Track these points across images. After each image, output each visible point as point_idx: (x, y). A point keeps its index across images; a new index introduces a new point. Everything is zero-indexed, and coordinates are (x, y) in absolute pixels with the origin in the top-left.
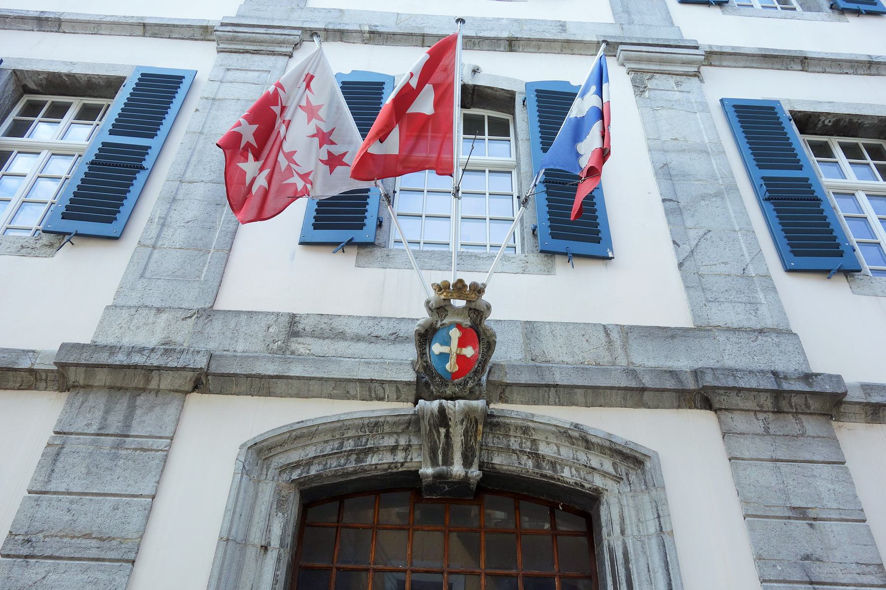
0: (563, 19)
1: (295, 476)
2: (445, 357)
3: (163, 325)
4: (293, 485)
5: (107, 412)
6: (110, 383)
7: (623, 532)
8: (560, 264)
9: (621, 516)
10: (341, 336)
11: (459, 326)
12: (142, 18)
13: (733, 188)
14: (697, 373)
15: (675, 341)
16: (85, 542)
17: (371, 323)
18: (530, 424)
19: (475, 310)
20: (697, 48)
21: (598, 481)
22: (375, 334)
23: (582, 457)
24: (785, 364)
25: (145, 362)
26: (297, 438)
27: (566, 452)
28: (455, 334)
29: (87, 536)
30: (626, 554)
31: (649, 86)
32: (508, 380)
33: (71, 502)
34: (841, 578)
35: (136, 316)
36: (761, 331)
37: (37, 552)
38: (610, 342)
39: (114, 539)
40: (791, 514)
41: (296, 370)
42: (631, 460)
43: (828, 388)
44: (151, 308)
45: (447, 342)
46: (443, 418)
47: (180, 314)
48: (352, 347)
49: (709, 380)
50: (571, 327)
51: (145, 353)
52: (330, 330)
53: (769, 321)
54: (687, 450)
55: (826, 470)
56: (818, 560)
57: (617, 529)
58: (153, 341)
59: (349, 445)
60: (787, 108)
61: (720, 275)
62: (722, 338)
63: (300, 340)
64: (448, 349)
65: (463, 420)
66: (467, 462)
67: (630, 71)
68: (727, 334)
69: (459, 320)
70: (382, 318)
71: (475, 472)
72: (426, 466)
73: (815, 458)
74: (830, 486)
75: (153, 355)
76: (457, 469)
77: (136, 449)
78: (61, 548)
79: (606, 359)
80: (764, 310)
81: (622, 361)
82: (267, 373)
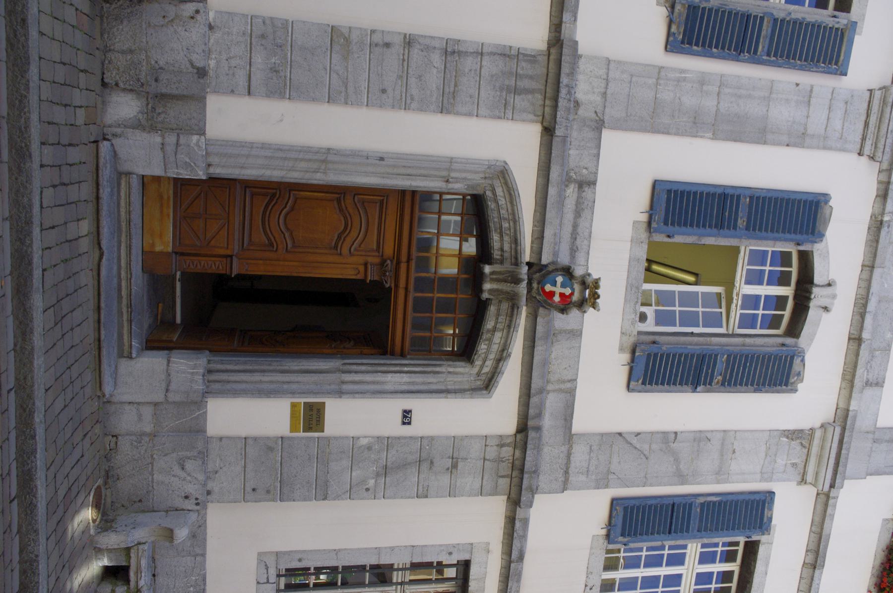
0: (885, 385)
1: (489, 193)
2: (554, 284)
5: (531, 78)
6: (546, 81)
7: (449, 372)
8: (626, 357)
9: (462, 373)
10: (578, 213)
11: (572, 294)
13: (683, 480)
14: (538, 429)
16: (453, 84)
17: (586, 234)
21: (478, 363)
23: (492, 356)
24: (543, 480)
26: (510, 194)
27: (495, 348)
28: (568, 291)
29: (456, 85)
30: (438, 373)
34: (422, 476)
36: (566, 472)
37: (449, 58)
38: (564, 382)
41: (552, 191)
42: (488, 385)
43: (523, 499)
45: (563, 285)
46: (517, 281)
47: (599, 109)
52: (582, 208)
53: (572, 478)
54: (492, 415)
55: (477, 485)
57: (451, 370)
58: (580, 95)
59: (505, 225)
60: (763, 539)
62: (564, 449)
63: (576, 190)
64: (558, 287)
66: (491, 291)
68: (566, 452)
70: (590, 242)
71: (485, 296)
75: (566, 101)
76: (487, 286)
77: (506, 100)
81: (550, 387)
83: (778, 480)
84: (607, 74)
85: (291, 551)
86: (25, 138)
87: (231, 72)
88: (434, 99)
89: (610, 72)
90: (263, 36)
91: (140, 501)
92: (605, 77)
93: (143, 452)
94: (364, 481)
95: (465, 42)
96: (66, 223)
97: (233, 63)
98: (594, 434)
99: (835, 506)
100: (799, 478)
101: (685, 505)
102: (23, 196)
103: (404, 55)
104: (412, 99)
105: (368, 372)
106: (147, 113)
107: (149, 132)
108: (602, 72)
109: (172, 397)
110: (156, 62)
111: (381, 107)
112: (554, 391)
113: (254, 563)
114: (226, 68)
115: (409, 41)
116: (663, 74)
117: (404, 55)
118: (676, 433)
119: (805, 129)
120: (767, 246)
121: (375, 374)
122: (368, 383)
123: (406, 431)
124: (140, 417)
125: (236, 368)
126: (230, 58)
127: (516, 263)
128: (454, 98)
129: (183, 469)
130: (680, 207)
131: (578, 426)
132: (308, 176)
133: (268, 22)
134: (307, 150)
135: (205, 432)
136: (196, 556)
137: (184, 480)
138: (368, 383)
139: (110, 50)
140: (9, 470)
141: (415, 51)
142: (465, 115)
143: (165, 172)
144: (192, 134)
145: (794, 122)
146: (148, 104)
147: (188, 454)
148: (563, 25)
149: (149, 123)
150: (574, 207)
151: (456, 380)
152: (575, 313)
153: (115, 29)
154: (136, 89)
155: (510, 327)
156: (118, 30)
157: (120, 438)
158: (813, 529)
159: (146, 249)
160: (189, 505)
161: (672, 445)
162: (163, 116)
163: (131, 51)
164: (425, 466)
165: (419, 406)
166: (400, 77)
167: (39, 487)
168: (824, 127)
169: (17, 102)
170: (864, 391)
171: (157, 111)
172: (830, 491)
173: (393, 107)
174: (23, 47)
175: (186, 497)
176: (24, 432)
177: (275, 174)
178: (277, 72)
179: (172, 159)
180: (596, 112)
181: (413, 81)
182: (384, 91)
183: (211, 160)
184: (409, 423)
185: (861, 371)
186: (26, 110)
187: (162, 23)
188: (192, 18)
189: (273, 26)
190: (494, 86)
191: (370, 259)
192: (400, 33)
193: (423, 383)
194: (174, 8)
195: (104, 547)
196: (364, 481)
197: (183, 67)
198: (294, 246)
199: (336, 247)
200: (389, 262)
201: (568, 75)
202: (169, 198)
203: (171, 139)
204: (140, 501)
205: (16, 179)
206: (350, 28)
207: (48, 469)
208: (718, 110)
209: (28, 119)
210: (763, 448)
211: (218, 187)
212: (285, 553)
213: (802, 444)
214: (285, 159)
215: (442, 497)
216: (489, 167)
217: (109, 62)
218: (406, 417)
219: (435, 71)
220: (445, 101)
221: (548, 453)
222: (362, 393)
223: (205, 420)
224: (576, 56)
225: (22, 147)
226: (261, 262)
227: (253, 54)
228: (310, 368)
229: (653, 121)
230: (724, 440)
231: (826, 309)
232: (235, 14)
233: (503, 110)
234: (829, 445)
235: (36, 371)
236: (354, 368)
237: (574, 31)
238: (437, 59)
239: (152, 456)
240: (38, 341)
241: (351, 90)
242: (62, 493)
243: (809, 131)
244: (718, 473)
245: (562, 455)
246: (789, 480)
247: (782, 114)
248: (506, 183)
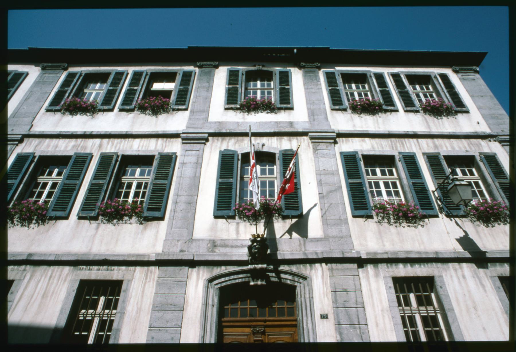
0: (292, 121)
17: (235, 241)
29: (171, 305)
88: (177, 314)
112: (305, 248)
118: (319, 194)
120: (147, 199)
123: (331, 316)
130: (227, 204)
161: (324, 195)
164: (347, 305)
166: (167, 330)
181: (169, 325)
184: (327, 315)
208: (186, 195)
218: (324, 316)
220: (178, 309)
233: (184, 284)
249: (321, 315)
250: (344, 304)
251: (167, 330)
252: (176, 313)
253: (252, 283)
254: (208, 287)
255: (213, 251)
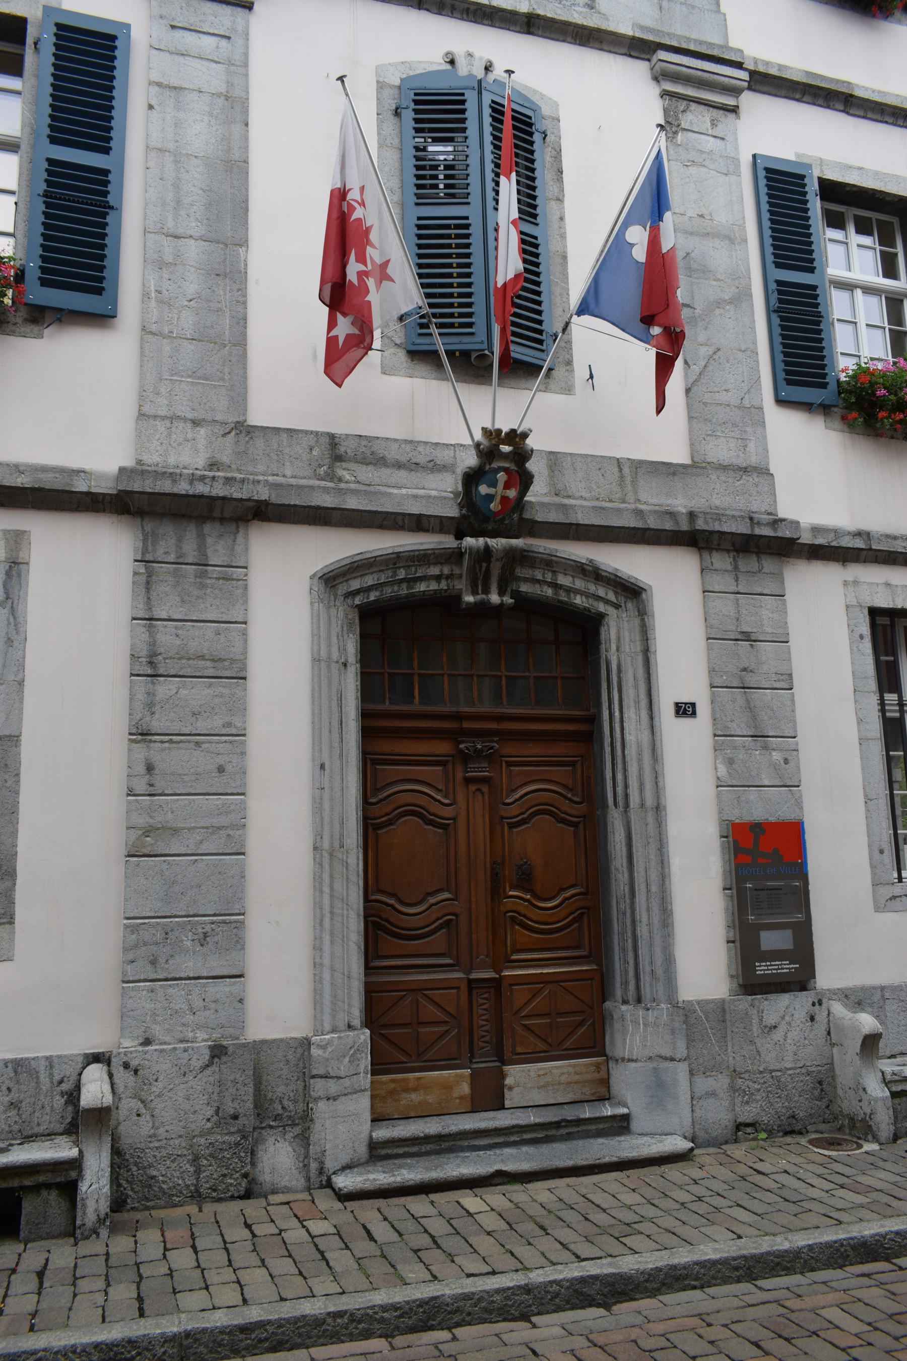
1: (357, 601)
2: (490, 498)
3: (204, 442)
4: (356, 610)
6: (181, 517)
9: (617, 631)
10: (380, 461)
11: (506, 470)
12: (617, 570)
13: (743, 296)
14: (692, 516)
15: (676, 478)
17: (408, 448)
18: (554, 558)
19: (520, 454)
20: (739, 65)
21: (602, 607)
22: (414, 460)
23: (592, 588)
24: (758, 505)
25: (210, 492)
27: (579, 584)
28: (502, 476)
29: (202, 657)
31: (683, 126)
32: (540, 517)
33: (176, 628)
35: (174, 429)
36: (745, 470)
37: (161, 671)
38: (622, 477)
39: (224, 660)
40: (739, 637)
42: (632, 592)
44: (185, 420)
45: (493, 484)
48: (394, 475)
49: (700, 525)
50: (589, 459)
51: (207, 481)
53: (753, 460)
54: (673, 584)
56: (751, 671)
59: (402, 574)
60: (816, 173)
61: (721, 404)
63: (344, 465)
65: (502, 558)
66: (501, 593)
67: (665, 94)
68: (718, 472)
69: (506, 465)
70: (418, 442)
72: (467, 595)
73: (766, 591)
74: (770, 615)
76: (495, 598)
77: (218, 579)
78: (181, 669)
79: (617, 496)
80: (751, 446)
82: (325, 505)
83: (737, 148)
84: (164, 418)
85: (871, 864)
86: (411, 1309)
87: (213, 1005)
88: (226, 691)
89: (160, 413)
90: (154, 962)
91: (820, 1083)
92: (168, 422)
93: (756, 1086)
94: (775, 767)
95: (133, 647)
96: (489, 1233)
97: (198, 1003)
98: (691, 431)
99: (767, 63)
100: (731, 116)
101: (780, 292)
102: (493, 1302)
103: (162, 742)
104: (229, 725)
105: (625, 770)
106: (284, 1127)
107: (312, 1120)
108: (161, 426)
109: (681, 1051)
110: (208, 1120)
111: (245, 773)
112: (636, 493)
113: (889, 917)
114: (207, 1013)
115: (142, 734)
116: (154, 328)
117: (162, 742)
119: (219, 95)
121: (628, 758)
122: (640, 769)
124: (713, 1094)
125: (631, 961)
126: (191, 1009)
127: (457, 556)
128: (221, 660)
129: (775, 1027)
131: (679, 455)
132: (353, 878)
133: (131, 956)
134: (317, 880)
135: (723, 1001)
136: (885, 999)
137: (789, 1024)
138: (640, 769)
139: (197, 1191)
140: (863, 1275)
141: (158, 724)
142: (246, 641)
143: (365, 1090)
144: (310, 1056)
145: (211, 114)
146: (271, 1127)
147: (755, 1021)
148: (93, 490)
149: (301, 1124)
150: (370, 467)
151: (627, 639)
152: (531, 465)
153: (165, 1186)
154: (251, 1150)
155: (550, 563)
156: (164, 1182)
157: (740, 1120)
158: (797, 96)
159: (468, 1106)
160: (821, 1016)
161: (698, 311)
162: (286, 1103)
163: (196, 1159)
164: (751, 680)
165: (668, 695)
167: (872, 1232)
168: (214, 65)
169: (360, 1326)
170: (603, 11)
171: (280, 1112)
172: (746, 70)
173: (243, 753)
174: (280, 1326)
175: (812, 1019)
176: (806, 1262)
177: (354, 927)
178: (205, 935)
179: (347, 1082)
180: (224, 435)
181: (202, 725)
182: (221, 770)
183: (342, 1025)
184: (693, 705)
185: (576, 15)
186: (370, 1312)
187: (148, 1117)
188: (136, 1071)
189: (136, 946)
190: (198, 597)
191: (460, 774)
192: (130, 750)
193: (636, 687)
194: (123, 1101)
195: (892, 1128)
196: (775, 767)
197: (212, 1079)
198: (448, 890)
199: (444, 827)
200: (462, 746)
201: (174, 481)
202: (393, 1081)
203: (319, 1087)
204: (820, 1083)
205: (469, 1314)
206: (128, 828)
207: (840, 1223)
209: (385, 1308)
210: (693, 170)
211: (380, 1009)
212: (874, 874)
213: (683, 112)
214: (332, 913)
215: (789, 653)
216: (322, 601)
217: (215, 1190)
218: (685, 710)
219: (183, 692)
221: (720, 501)
222: (657, 777)
223: (708, 1002)
224: (138, 471)
225: (424, 1312)
226: (474, 936)
227: (183, 975)
228: (624, 853)
229: (226, 344)
230: (686, 232)
231: (488, 68)
232: (123, 1006)
233: (234, 579)
234: (684, 69)
235: (725, 1255)
236: (620, 790)
237: (101, 476)
238: (165, 688)
239: (761, 1072)
240: (683, 1257)
241: (223, 821)
242: (859, 1199)
243: (223, 89)
244: (732, 241)
245: (723, 478)
246: (735, 133)
247: (200, 134)
248: (343, 574)
249: (677, 705)
250: (741, 679)
251: (198, 744)
252: (222, 688)
253: (469, 599)
254: (148, 585)
255: (331, 476)
